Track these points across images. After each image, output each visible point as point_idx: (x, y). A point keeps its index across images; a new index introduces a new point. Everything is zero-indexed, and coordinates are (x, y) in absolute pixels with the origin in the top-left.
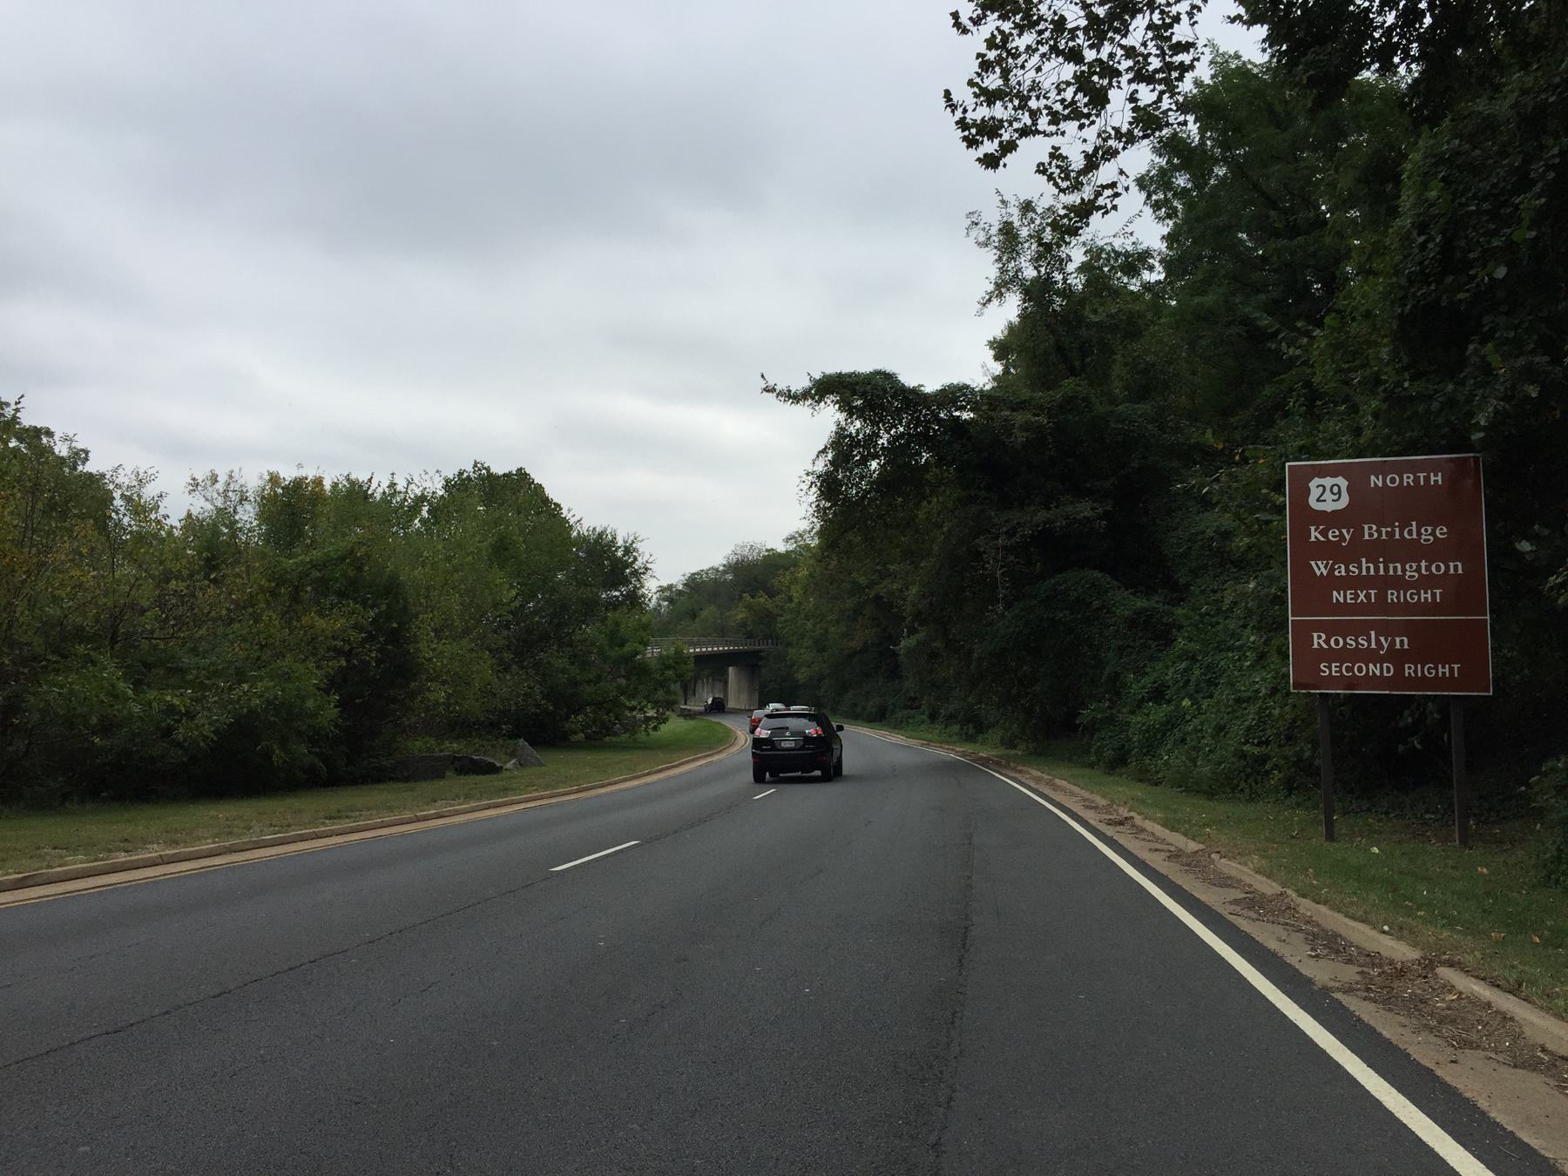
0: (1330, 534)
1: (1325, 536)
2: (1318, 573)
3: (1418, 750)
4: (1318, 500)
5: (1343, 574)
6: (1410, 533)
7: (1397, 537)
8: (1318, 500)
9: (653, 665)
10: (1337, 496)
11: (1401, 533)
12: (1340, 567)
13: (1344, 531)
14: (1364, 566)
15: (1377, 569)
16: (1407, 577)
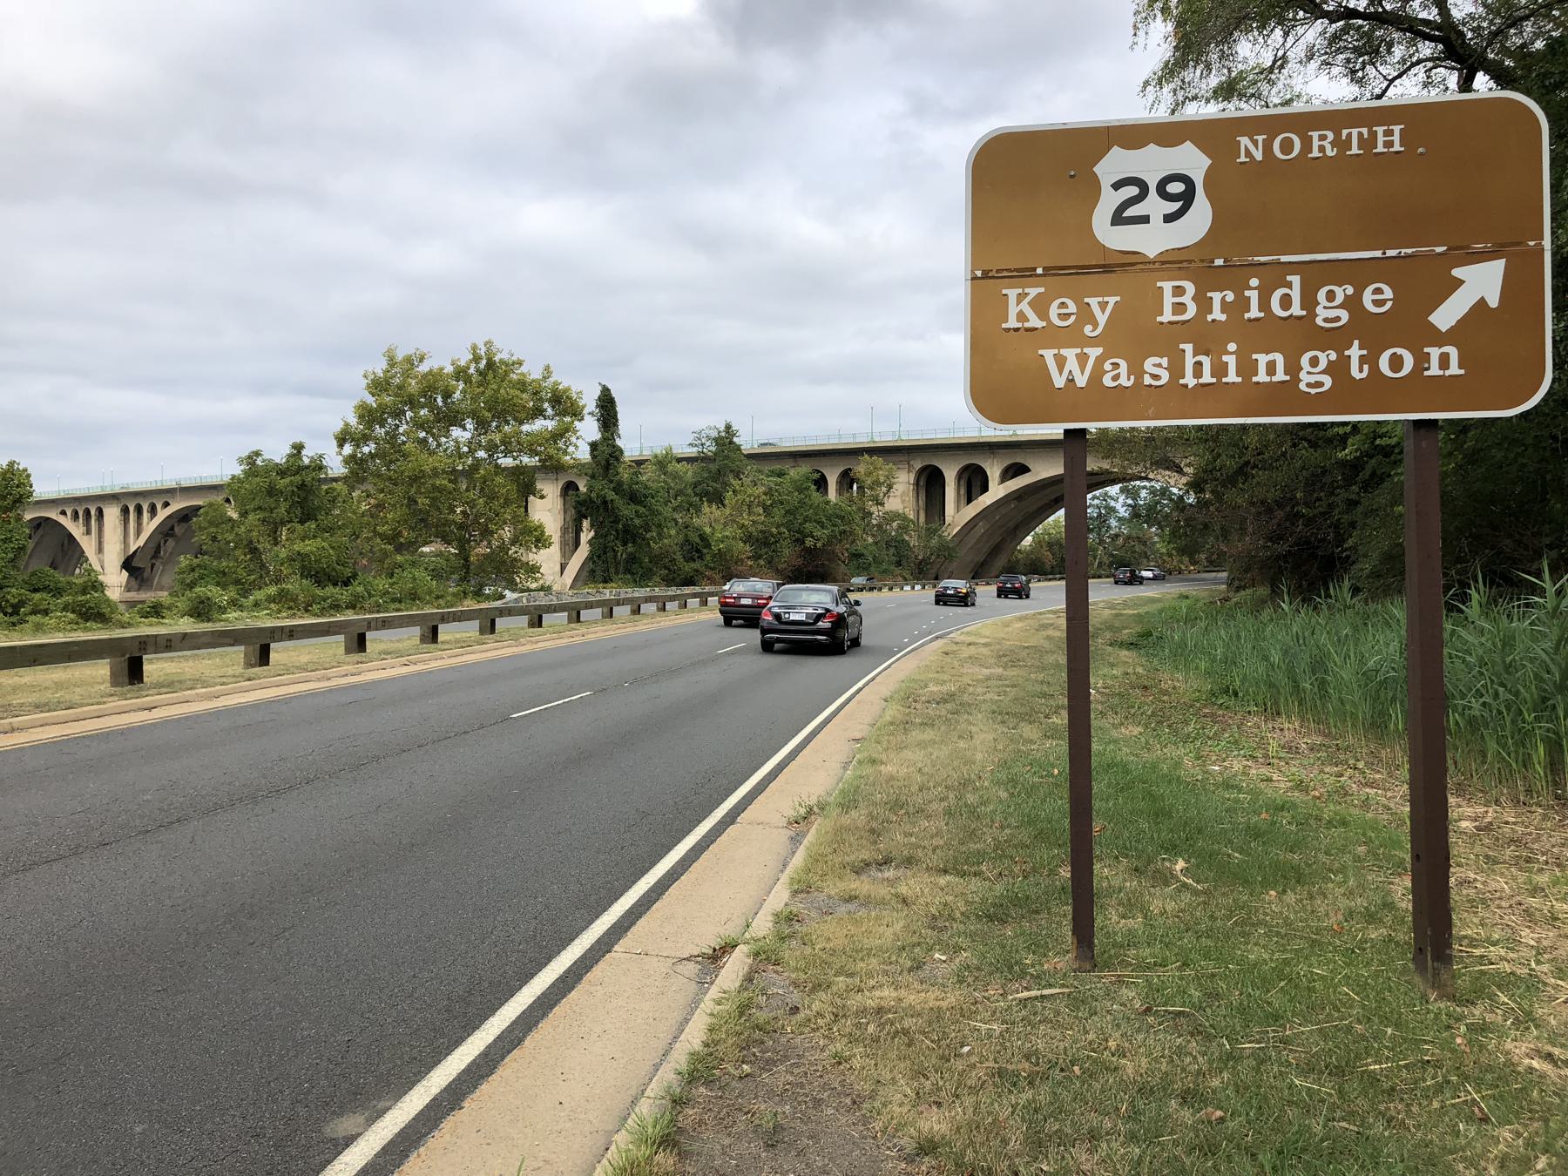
0: (1054, 311)
1: (1043, 314)
2: (1059, 382)
3: (826, 644)
4: (1118, 219)
5: (1125, 381)
6: (1286, 302)
7: (1254, 312)
8: (1118, 219)
9: (455, 543)
10: (1177, 205)
11: (1264, 304)
12: (1116, 366)
13: (1093, 302)
14: (1189, 361)
15: (1220, 370)
16: (1302, 386)
